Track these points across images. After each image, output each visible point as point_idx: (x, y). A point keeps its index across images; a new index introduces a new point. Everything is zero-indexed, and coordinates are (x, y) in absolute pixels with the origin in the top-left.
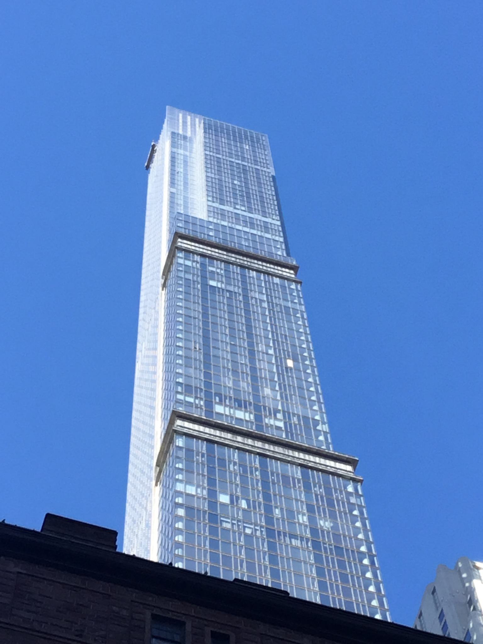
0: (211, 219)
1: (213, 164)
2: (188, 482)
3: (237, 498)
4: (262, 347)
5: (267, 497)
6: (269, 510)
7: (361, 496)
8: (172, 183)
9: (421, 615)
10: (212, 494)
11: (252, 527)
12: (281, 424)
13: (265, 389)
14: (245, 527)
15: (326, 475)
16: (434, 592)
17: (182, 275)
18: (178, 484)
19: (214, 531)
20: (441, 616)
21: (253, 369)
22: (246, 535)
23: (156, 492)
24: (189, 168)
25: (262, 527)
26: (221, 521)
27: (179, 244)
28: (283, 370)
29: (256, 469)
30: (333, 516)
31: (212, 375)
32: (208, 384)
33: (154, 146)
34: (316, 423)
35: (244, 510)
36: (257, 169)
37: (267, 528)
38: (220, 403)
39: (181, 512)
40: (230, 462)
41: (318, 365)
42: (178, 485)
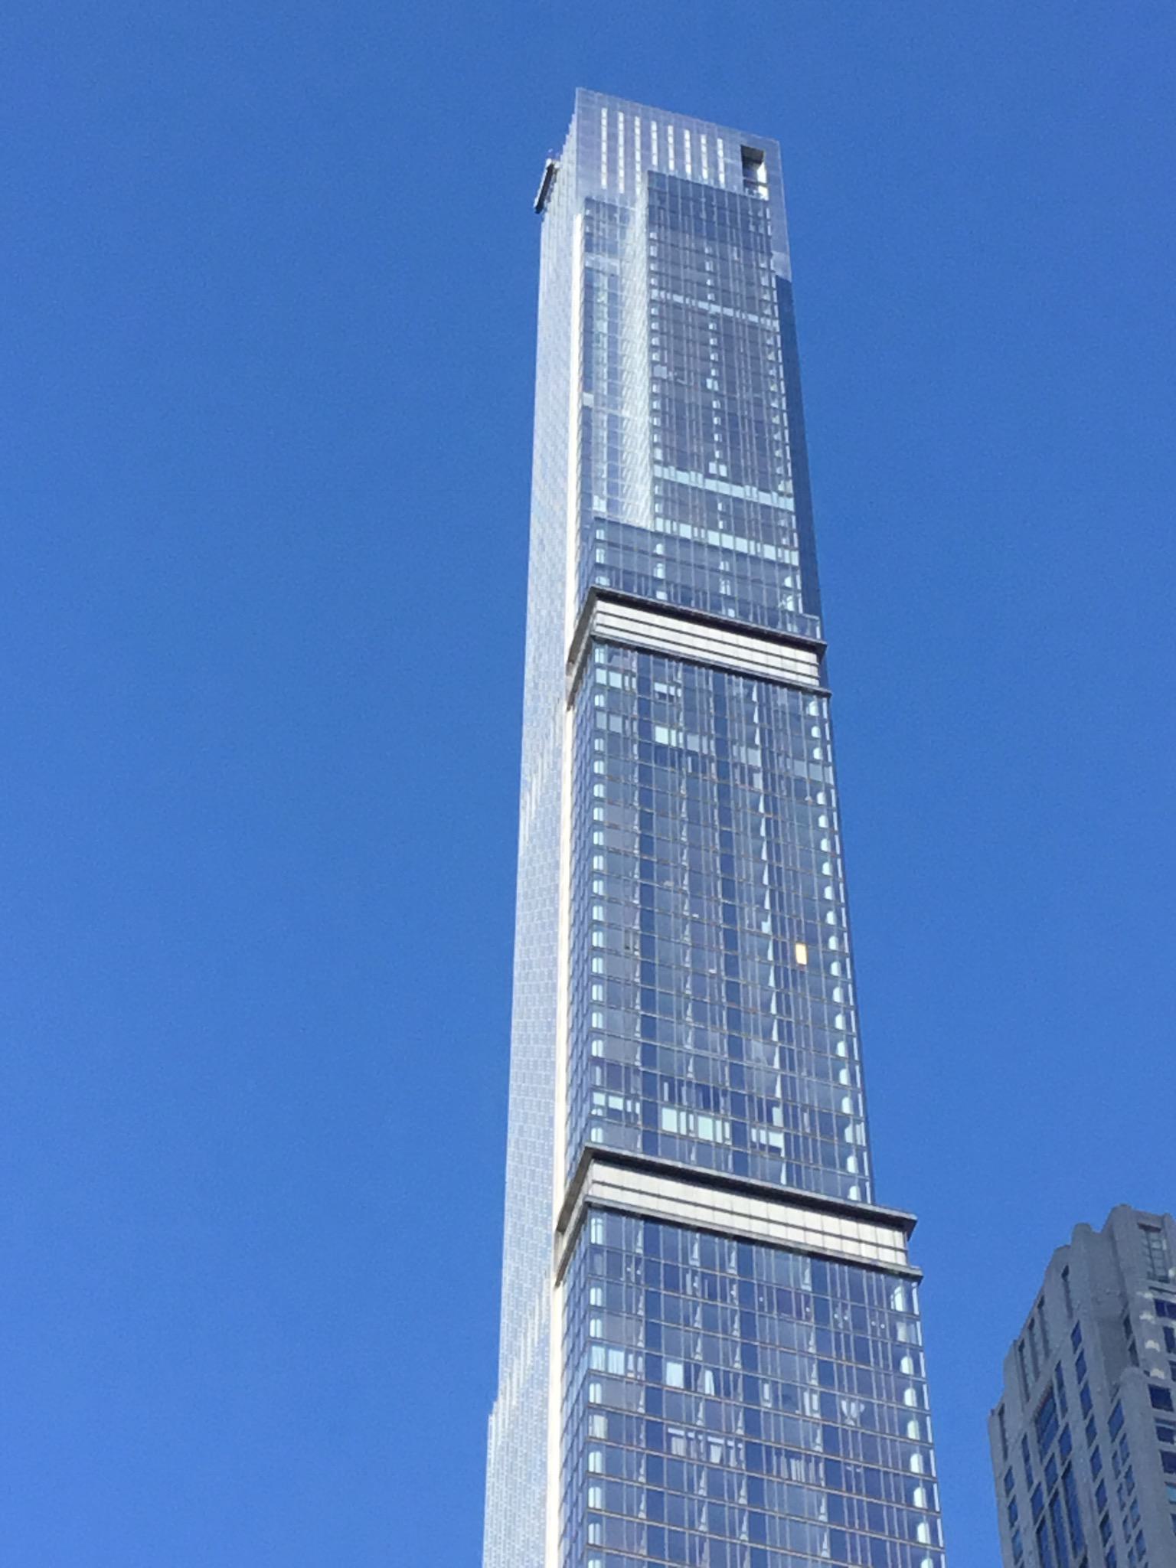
0: (660, 525)
1: (672, 327)
2: (609, 1343)
3: (698, 1368)
4: (750, 912)
5: (750, 1357)
6: (752, 1392)
7: (918, 1318)
8: (587, 382)
10: (654, 1368)
13: (753, 1042)
17: (602, 721)
18: (598, 671)
20: (1076, 1335)
21: (733, 989)
23: (568, 720)
26: (670, 1436)
30: (865, 1389)
32: (649, 1054)
34: (843, 1121)
36: (753, 326)
38: (674, 1100)
39: (599, 1426)
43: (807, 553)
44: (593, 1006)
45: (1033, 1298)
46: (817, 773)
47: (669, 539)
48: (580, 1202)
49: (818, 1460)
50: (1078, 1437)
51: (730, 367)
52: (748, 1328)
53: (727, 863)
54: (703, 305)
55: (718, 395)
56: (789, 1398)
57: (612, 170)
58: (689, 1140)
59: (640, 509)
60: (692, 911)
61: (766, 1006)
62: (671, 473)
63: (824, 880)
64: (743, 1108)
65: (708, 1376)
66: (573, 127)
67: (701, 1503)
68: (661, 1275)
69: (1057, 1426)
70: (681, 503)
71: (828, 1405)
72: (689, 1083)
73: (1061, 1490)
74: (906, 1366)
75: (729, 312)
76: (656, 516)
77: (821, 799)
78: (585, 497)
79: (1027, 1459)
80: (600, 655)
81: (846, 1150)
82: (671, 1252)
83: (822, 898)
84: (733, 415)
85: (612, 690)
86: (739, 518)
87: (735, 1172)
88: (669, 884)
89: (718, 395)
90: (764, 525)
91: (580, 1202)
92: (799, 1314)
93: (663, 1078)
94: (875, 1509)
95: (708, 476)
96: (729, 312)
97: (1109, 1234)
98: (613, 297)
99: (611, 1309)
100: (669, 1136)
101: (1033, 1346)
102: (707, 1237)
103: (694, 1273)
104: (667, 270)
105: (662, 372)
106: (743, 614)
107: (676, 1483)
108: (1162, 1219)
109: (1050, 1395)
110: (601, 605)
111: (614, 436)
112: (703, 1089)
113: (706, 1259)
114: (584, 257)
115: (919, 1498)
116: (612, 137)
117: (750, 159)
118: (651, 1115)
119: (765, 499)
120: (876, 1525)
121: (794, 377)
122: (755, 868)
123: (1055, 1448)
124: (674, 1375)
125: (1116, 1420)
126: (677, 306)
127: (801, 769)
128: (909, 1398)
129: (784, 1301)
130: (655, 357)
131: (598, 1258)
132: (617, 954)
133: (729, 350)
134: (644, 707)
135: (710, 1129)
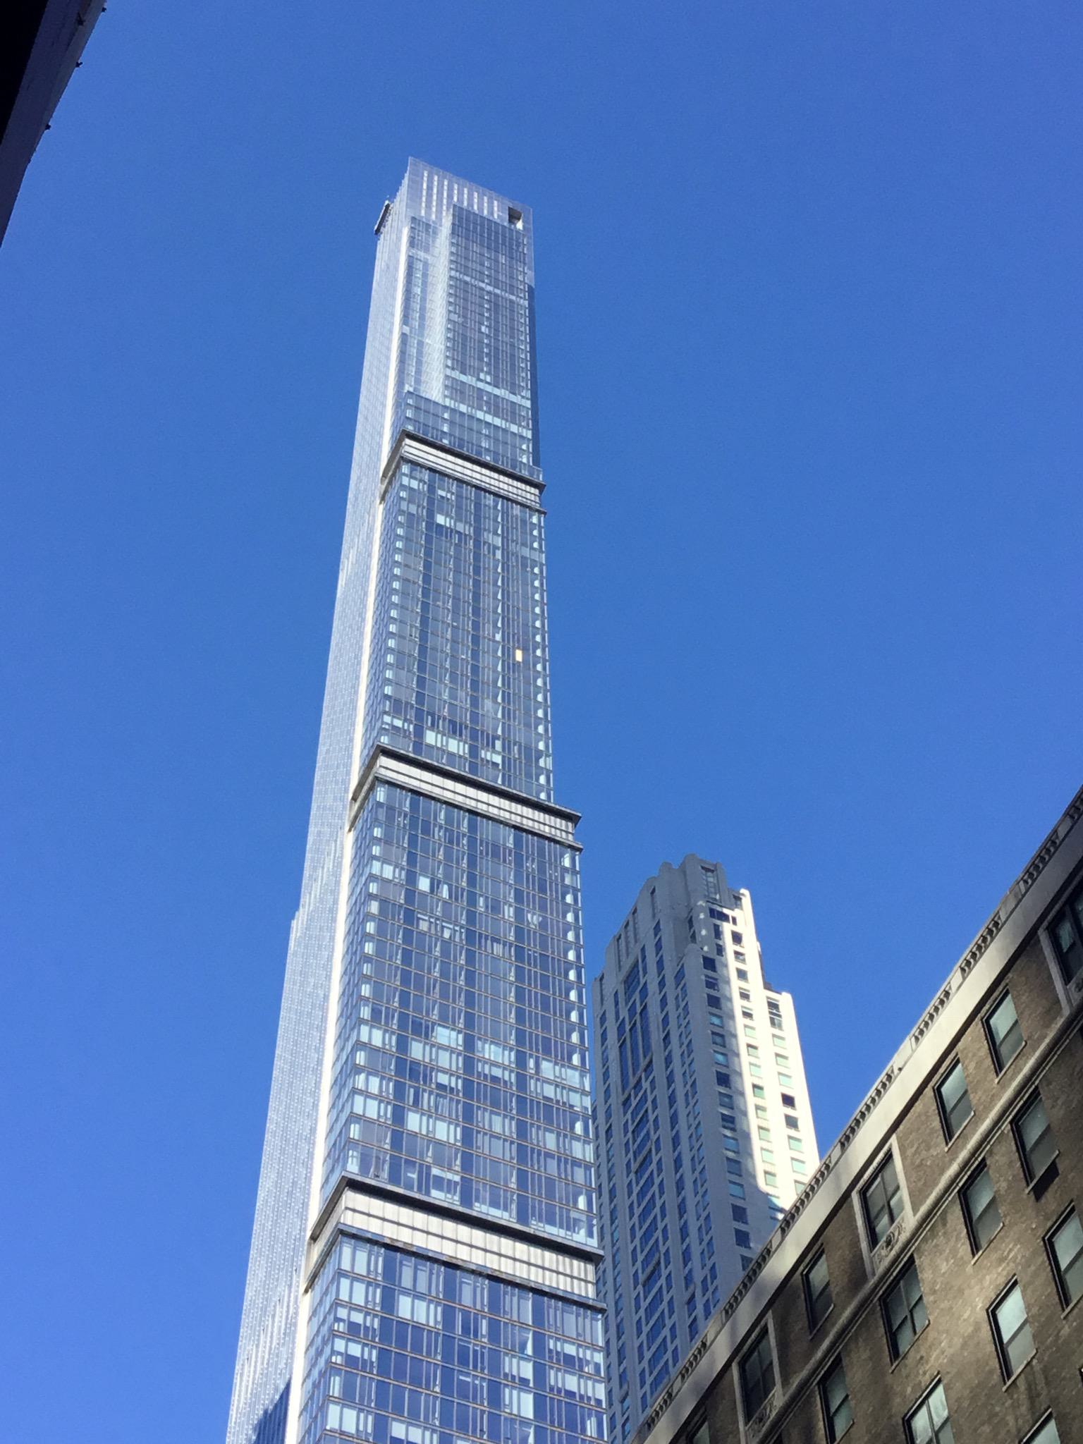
0: (448, 402)
1: (461, 293)
2: (385, 860)
3: (439, 882)
4: (488, 629)
5: (472, 880)
6: (472, 901)
8: (406, 319)
10: (412, 879)
17: (404, 506)
19: (408, 936)
20: (657, 929)
21: (475, 669)
22: (444, 942)
23: (380, 510)
24: (429, 289)
26: (419, 919)
27: (407, 448)
28: (510, 665)
29: (464, 835)
30: (543, 908)
32: (420, 697)
33: (388, 206)
34: (539, 754)
35: (445, 902)
36: (511, 301)
38: (433, 726)
39: (374, 907)
40: (435, 825)
41: (552, 660)
43: (535, 431)
44: (369, 917)
45: (630, 909)
46: (536, 556)
47: (453, 411)
48: (371, 778)
49: (511, 945)
50: (653, 987)
51: (497, 322)
52: (472, 863)
53: (476, 597)
54: (483, 285)
55: (488, 336)
56: (495, 907)
57: (429, 206)
58: (442, 750)
59: (435, 390)
60: (453, 620)
61: (495, 681)
62: (456, 374)
63: (535, 617)
64: (478, 738)
65: (446, 887)
66: (405, 181)
67: (436, 959)
68: (419, 827)
69: (639, 982)
70: (462, 393)
71: (519, 914)
72: (444, 719)
73: (628, 1041)
74: (569, 899)
75: (498, 291)
76: (446, 396)
77: (536, 570)
78: (400, 383)
79: (617, 1004)
80: (405, 469)
81: (540, 771)
82: (427, 813)
83: (534, 627)
84: (496, 349)
85: (409, 514)
86: (495, 406)
87: (470, 772)
88: (440, 603)
89: (488, 336)
90: (513, 413)
91: (371, 778)
92: (505, 861)
93: (428, 713)
94: (545, 979)
95: (479, 380)
96: (498, 291)
97: (683, 870)
98: (425, 275)
99: (386, 841)
100: (429, 746)
101: (627, 937)
102: (450, 808)
103: (441, 827)
104: (460, 261)
105: (455, 317)
106: (496, 460)
107: (421, 945)
108: (715, 866)
109: (636, 965)
110: (408, 441)
111: (420, 353)
112: (452, 722)
113: (449, 820)
114: (408, 250)
115: (572, 975)
116: (430, 188)
117: (513, 216)
118: (419, 732)
119: (513, 398)
120: (545, 986)
121: (540, 328)
122: (493, 601)
123: (637, 996)
124: (424, 884)
125: (680, 976)
126: (466, 283)
127: (526, 552)
128: (570, 917)
129: (495, 851)
130: (451, 308)
131: (380, 810)
132: (404, 638)
133: (496, 313)
134: (431, 501)
135: (454, 746)
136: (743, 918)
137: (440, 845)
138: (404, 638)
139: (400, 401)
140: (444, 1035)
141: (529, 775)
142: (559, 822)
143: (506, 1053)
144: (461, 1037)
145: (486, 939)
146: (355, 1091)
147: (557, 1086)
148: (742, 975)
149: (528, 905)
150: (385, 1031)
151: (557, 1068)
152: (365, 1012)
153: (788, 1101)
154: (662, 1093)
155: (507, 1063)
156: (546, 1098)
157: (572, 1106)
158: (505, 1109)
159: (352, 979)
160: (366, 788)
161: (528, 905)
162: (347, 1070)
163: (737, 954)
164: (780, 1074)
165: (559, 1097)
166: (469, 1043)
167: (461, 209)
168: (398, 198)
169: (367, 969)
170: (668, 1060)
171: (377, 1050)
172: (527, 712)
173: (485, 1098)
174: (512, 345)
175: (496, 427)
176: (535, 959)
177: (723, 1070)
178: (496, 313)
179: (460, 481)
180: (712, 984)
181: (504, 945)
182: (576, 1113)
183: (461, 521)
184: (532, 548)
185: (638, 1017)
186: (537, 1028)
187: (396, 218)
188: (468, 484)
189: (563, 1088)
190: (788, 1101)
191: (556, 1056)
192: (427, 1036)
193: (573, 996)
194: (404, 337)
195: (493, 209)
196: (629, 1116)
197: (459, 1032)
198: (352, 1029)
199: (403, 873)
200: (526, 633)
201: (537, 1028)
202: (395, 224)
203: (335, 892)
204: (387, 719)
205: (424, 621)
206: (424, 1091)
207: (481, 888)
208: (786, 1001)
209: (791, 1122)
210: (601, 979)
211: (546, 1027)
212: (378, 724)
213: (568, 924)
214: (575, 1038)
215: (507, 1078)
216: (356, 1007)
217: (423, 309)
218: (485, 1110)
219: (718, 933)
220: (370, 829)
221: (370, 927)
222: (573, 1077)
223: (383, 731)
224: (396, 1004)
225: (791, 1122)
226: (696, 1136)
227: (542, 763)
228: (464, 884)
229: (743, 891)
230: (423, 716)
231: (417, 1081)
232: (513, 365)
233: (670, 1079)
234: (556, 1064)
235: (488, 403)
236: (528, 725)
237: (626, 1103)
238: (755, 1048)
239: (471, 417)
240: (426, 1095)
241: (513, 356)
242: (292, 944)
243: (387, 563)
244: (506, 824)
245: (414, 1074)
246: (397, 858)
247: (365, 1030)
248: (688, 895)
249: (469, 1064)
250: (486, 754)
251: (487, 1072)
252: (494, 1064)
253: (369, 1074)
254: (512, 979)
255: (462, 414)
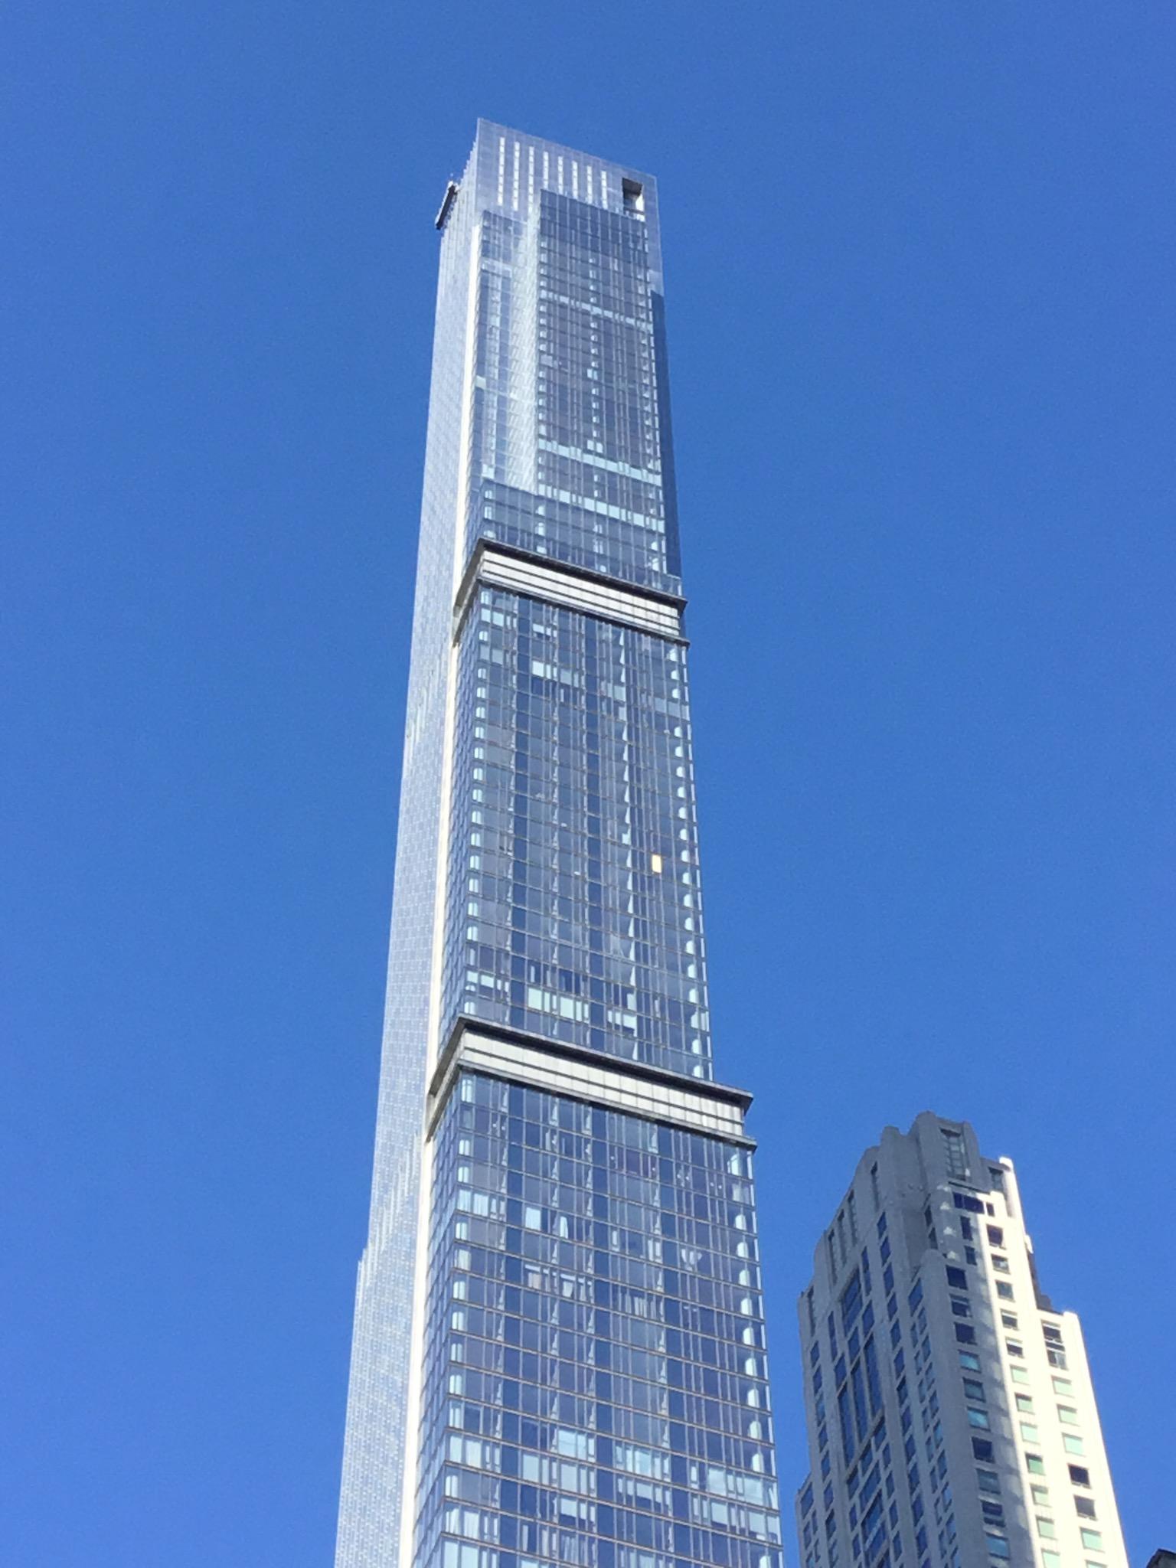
0: (542, 490)
1: (557, 324)
2: (475, 1188)
3: (554, 1213)
5: (600, 1208)
6: (602, 1238)
8: (480, 366)
9: (851, 1197)
10: (515, 1212)
11: (573, 1278)
12: (631, 1022)
14: (562, 1280)
15: (697, 1138)
16: (874, 1170)
17: (485, 653)
20: (882, 1224)
21: (595, 891)
23: (453, 655)
25: (588, 1278)
27: (486, 566)
28: (645, 880)
29: (587, 1141)
30: (702, 1240)
31: (529, 760)
32: (518, 941)
34: (690, 1009)
36: (630, 328)
37: (597, 1281)
38: (539, 982)
39: (463, 1260)
40: (545, 1130)
42: (464, 1196)
44: (455, 1305)
45: (846, 1192)
46: (675, 710)
47: (550, 502)
48: (453, 1064)
50: (880, 1312)
51: (608, 360)
52: (600, 1181)
54: (587, 307)
55: (598, 384)
56: (635, 1244)
57: (508, 190)
58: (552, 1017)
59: (524, 475)
60: (561, 820)
61: (624, 907)
64: (602, 994)
65: (563, 1221)
68: (523, 1133)
71: (669, 1251)
72: (554, 969)
74: (740, 1222)
75: (609, 314)
76: (540, 482)
77: (678, 732)
78: (476, 463)
79: (832, 1333)
80: (485, 597)
81: (692, 1034)
82: (533, 1113)
86: (612, 488)
87: (593, 1046)
89: (598, 384)
90: (634, 496)
91: (453, 1064)
92: (646, 1174)
94: (708, 1346)
97: (914, 1137)
98: (506, 297)
99: (478, 1159)
100: (534, 1012)
101: (842, 1236)
103: (553, 1132)
104: (553, 275)
105: (547, 360)
106: (614, 571)
107: (531, 1312)
108: (961, 1126)
109: (856, 1276)
110: (487, 555)
111: (502, 415)
112: (565, 973)
113: (565, 1120)
114: (481, 262)
116: (509, 163)
117: (630, 191)
118: (519, 993)
119: (636, 474)
120: (709, 1357)
122: (618, 783)
123: (859, 1322)
124: (532, 1219)
125: (915, 1297)
126: (562, 306)
127: (662, 706)
128: (742, 1250)
129: (633, 1161)
130: (543, 347)
133: (608, 346)
134: (523, 643)
135: (570, 1008)
136: (1004, 1212)
137: (554, 1159)
138: (493, 852)
139: (477, 486)
140: (570, 1443)
141: (676, 1043)
142: (725, 1110)
143: (658, 1461)
144: (592, 1442)
145: (624, 1292)
146: (445, 1537)
147: (731, 1505)
148: (1005, 1290)
149: (682, 1237)
150: (485, 1443)
151: (731, 1478)
152: (456, 1418)
153: (1079, 1475)
154: (898, 1466)
155: (658, 1476)
156: (716, 1525)
157: (753, 1534)
158: (659, 1547)
159: (438, 1369)
160: (447, 1078)
161: (682, 1237)
162: (435, 1505)
163: (997, 1259)
164: (1065, 1435)
165: (734, 1523)
166: (604, 1452)
167: (552, 195)
168: (465, 179)
169: (456, 1352)
170: (906, 1422)
171: (475, 1472)
172: (671, 945)
173: (630, 1531)
174: (633, 393)
175: (613, 521)
176: (697, 1322)
177: (984, 1436)
178: (608, 346)
179: (564, 608)
180: (960, 1308)
181: (649, 1300)
182: (760, 1544)
183: (567, 669)
184: (671, 700)
185: (861, 1354)
186: (699, 1421)
187: (464, 207)
188: (574, 610)
189: (740, 1507)
190: (1079, 1475)
191: (729, 1462)
192: (544, 1447)
193: (750, 1367)
194: (478, 393)
195: (595, 186)
196: (856, 1498)
197: (590, 1436)
198: (439, 1443)
199: (503, 1205)
200: (665, 829)
201: (699, 1421)
202: (463, 217)
203: (412, 1229)
204: (473, 977)
205: (520, 825)
206: (543, 1527)
207: (613, 1220)
208: (1069, 1324)
209: (1085, 1507)
210: (810, 1294)
211: (712, 1418)
212: (461, 983)
213: (740, 1260)
214: (754, 1430)
215: (659, 1499)
216: (443, 1411)
217: (504, 347)
218: (630, 1549)
219: (967, 1230)
220: (455, 1143)
221: (459, 1290)
222: (753, 1491)
223: (466, 995)
224: (499, 1402)
225: (1085, 1507)
226: (948, 1536)
227: (694, 1022)
228: (590, 1214)
229: (1005, 1161)
230: (522, 967)
231: (533, 1514)
232: (634, 423)
233: (909, 1449)
234: (729, 1472)
235: (600, 485)
236: (672, 967)
237: (851, 1480)
238: (1027, 1398)
239: (577, 509)
240: (546, 1534)
241: (633, 409)
242: (360, 1296)
243: (465, 742)
244: (646, 1119)
245: (528, 1508)
246: (493, 1184)
247: (456, 1443)
248: (923, 1176)
249: (605, 1482)
250: (614, 1017)
251: (631, 1492)
252: (639, 1479)
253: (464, 1509)
254: (662, 1350)
255: (563, 505)
